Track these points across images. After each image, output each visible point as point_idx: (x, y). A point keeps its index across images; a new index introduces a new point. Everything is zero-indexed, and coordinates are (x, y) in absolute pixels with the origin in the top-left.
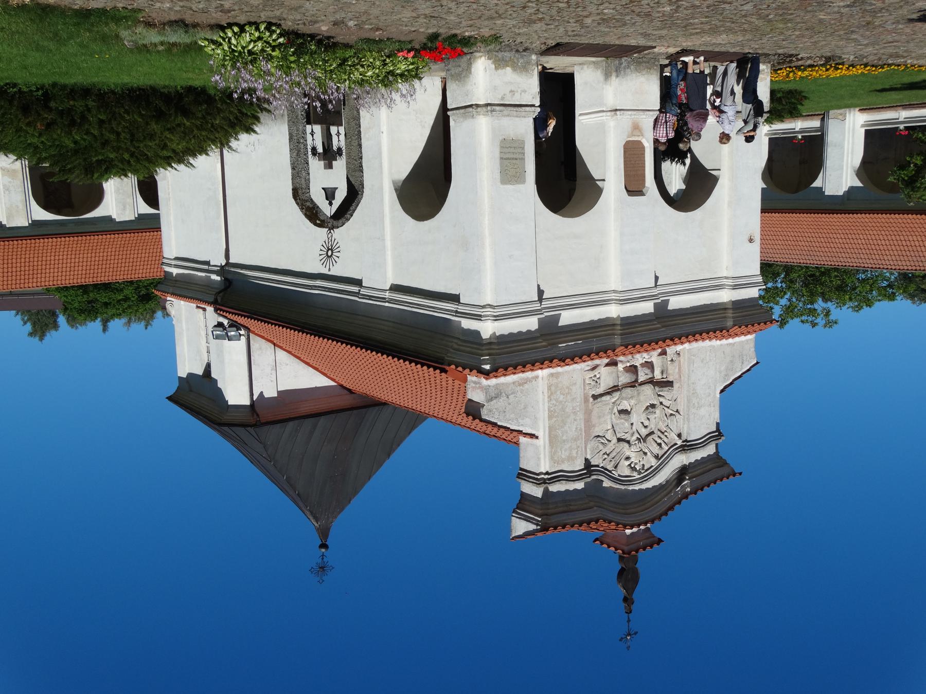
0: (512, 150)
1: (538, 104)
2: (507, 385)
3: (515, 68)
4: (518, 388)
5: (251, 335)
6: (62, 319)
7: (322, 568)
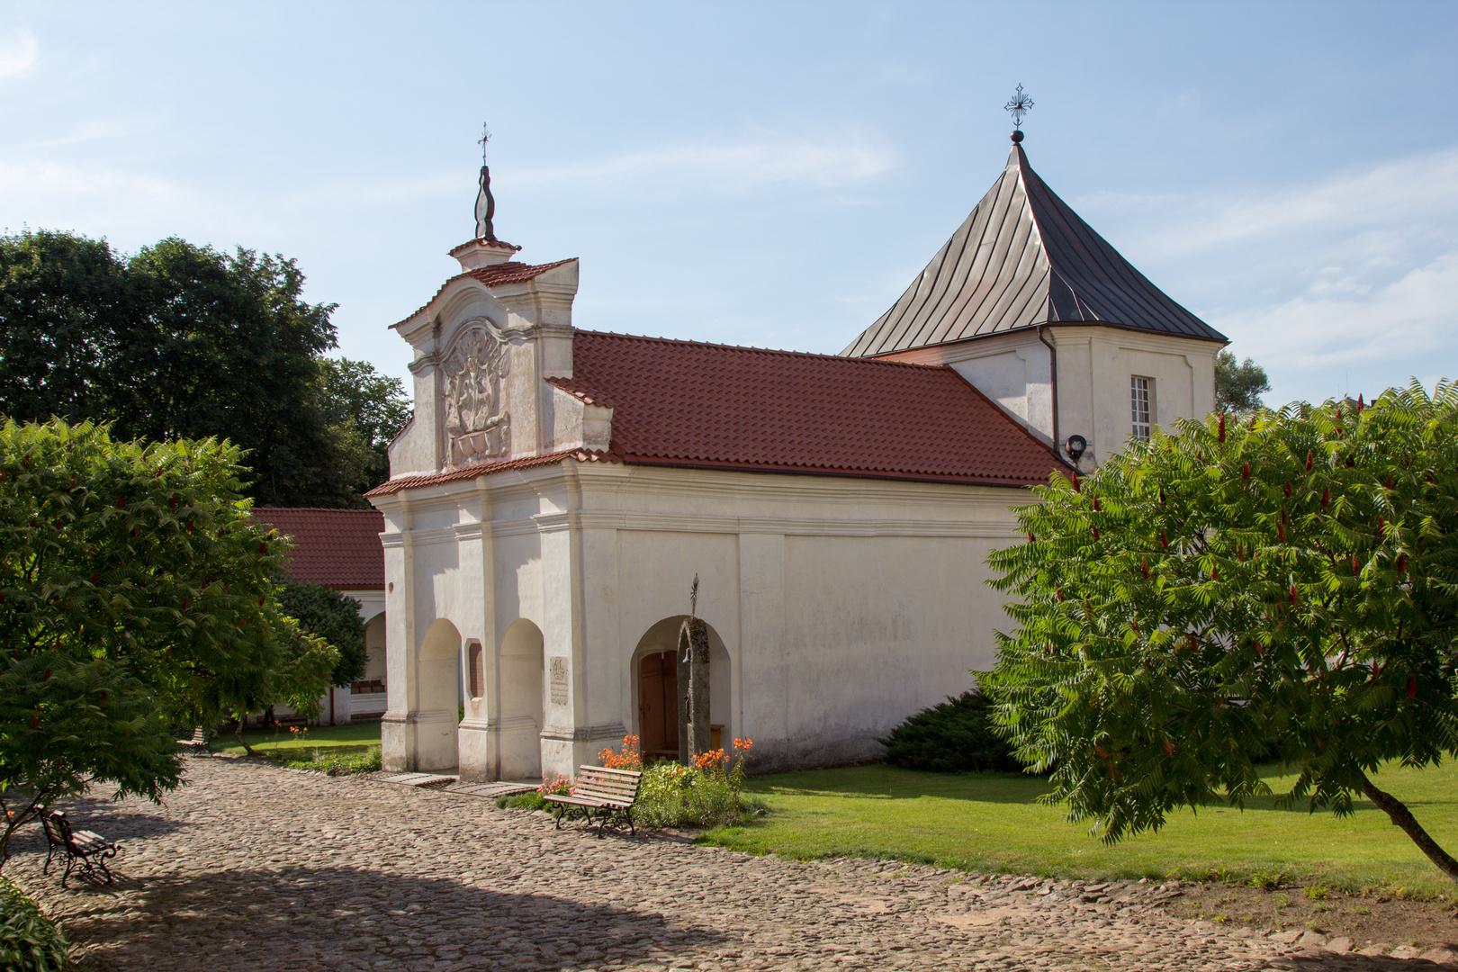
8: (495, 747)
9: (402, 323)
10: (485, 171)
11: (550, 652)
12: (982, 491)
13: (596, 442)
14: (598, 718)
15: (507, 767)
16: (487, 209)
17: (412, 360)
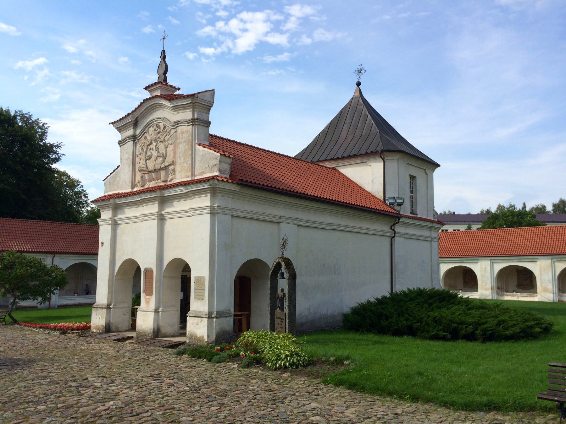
0: (200, 294)
1: (188, 318)
2: (209, 172)
3: (196, 336)
4: (204, 170)
5: (382, 199)
6: (549, 208)
7: (360, 72)
8: (156, 320)
9: (115, 122)
10: (164, 52)
11: (194, 275)
12: (366, 214)
13: (224, 174)
14: (222, 308)
15: (163, 330)
16: (164, 69)
17: (120, 139)
